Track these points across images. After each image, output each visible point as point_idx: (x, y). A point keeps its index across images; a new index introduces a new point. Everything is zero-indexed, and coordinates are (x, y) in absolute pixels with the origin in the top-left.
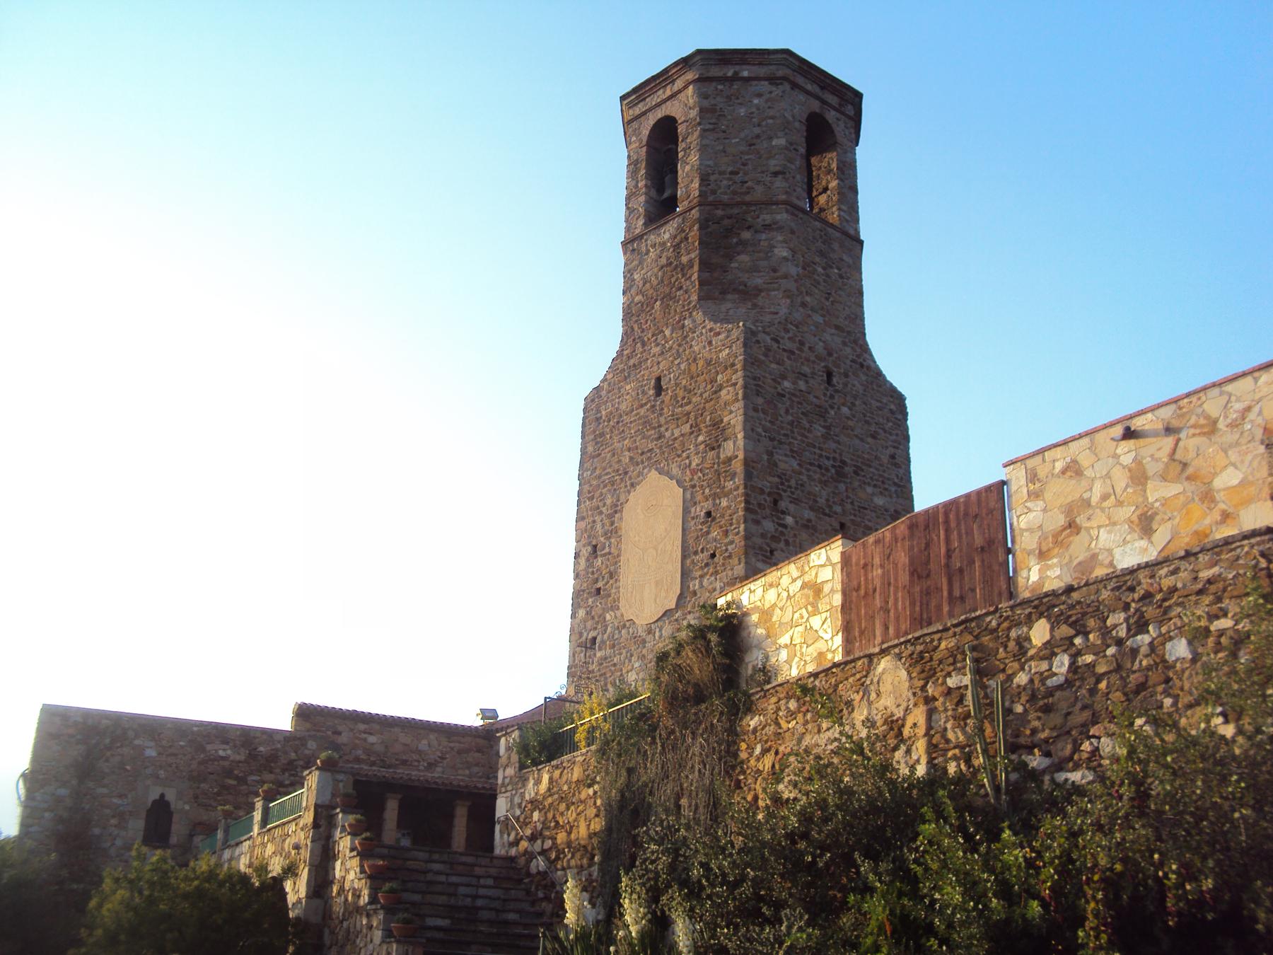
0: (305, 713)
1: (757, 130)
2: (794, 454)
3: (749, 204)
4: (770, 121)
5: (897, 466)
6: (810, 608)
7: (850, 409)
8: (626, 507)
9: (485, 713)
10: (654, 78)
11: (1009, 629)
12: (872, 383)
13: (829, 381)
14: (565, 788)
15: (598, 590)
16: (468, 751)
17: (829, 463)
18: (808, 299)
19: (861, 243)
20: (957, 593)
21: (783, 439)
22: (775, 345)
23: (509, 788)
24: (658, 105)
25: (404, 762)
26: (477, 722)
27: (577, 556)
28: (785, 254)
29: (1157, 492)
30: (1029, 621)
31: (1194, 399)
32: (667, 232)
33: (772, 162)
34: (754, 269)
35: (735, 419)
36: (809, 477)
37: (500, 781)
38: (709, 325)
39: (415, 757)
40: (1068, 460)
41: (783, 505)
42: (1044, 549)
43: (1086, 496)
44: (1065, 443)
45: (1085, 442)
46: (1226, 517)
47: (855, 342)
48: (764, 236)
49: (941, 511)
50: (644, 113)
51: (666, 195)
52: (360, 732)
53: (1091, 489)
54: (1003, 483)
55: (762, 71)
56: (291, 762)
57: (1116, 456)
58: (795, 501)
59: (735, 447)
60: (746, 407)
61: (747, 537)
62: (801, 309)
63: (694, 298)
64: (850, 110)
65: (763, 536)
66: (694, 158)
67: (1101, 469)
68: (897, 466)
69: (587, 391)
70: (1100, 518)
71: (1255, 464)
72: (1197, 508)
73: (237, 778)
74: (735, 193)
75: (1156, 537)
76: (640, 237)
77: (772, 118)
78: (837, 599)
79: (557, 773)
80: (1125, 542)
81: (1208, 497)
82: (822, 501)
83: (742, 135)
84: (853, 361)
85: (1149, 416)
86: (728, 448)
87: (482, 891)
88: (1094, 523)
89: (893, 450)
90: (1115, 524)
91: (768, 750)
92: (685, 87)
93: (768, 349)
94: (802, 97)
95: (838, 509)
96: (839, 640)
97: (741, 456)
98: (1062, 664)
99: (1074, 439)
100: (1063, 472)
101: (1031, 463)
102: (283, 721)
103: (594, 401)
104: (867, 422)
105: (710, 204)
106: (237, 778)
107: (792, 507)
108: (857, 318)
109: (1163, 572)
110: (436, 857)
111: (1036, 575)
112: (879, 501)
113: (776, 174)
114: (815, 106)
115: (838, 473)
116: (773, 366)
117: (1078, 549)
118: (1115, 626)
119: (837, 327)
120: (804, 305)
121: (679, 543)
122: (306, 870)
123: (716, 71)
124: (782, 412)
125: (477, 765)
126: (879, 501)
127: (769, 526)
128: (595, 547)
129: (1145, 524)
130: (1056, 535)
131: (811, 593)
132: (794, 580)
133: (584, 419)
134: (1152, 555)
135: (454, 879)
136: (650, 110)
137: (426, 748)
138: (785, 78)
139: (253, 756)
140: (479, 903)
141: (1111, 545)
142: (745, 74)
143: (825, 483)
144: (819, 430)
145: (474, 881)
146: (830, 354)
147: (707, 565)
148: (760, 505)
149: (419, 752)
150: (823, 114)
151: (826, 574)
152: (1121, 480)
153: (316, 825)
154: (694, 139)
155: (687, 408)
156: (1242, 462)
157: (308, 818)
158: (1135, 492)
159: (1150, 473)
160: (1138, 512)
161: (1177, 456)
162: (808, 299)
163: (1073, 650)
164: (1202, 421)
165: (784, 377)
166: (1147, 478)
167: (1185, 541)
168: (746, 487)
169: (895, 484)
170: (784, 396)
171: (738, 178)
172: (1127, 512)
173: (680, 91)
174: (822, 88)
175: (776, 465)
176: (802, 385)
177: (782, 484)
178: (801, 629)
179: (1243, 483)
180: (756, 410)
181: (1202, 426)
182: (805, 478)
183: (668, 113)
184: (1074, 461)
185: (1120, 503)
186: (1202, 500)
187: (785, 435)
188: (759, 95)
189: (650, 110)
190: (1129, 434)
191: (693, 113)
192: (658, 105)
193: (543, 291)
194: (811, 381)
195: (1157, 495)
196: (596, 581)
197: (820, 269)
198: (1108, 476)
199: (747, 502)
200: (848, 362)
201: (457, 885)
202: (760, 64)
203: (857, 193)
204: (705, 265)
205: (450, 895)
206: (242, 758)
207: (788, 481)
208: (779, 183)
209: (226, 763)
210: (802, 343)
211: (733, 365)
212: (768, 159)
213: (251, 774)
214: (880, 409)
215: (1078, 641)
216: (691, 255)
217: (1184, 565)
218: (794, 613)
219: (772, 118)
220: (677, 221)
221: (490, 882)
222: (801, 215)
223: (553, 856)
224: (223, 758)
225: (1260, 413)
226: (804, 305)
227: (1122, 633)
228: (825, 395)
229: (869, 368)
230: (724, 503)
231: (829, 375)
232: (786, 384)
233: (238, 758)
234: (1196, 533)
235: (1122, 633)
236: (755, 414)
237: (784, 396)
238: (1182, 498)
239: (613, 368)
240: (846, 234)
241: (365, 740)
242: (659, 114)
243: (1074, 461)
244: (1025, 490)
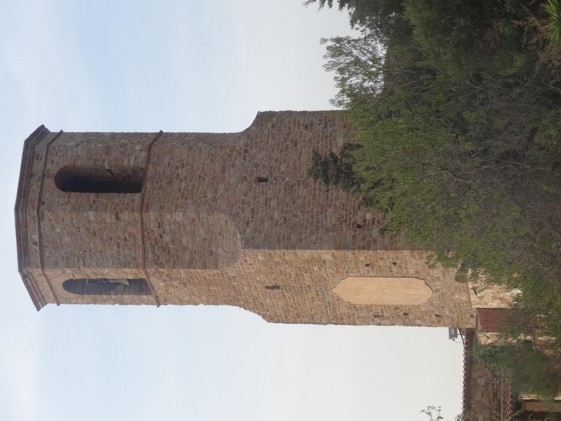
1: (83, 230)
3: (143, 232)
4: (74, 221)
7: (281, 163)
8: (352, 302)
10: (30, 294)
12: (256, 143)
13: (265, 180)
15: (404, 314)
21: (315, 219)
22: (251, 224)
25: (495, 395)
27: (380, 325)
28: (181, 214)
32: (154, 281)
33: (108, 220)
35: (306, 254)
36: (337, 199)
38: (237, 265)
39: (490, 387)
41: (360, 222)
48: (167, 228)
59: (326, 255)
60: (300, 248)
62: (219, 202)
63: (215, 271)
69: (265, 322)
74: (134, 245)
76: (157, 297)
77: (72, 219)
84: (244, 159)
89: (301, 127)
93: (255, 230)
103: (272, 317)
104: (287, 148)
105: (144, 261)
113: (118, 218)
114: (50, 183)
116: (266, 225)
119: (223, 172)
120: (215, 199)
121: (383, 279)
124: (297, 220)
128: (375, 316)
137: (483, 379)
142: (36, 237)
147: (400, 267)
148: (364, 239)
165: (272, 218)
168: (354, 249)
169: (325, 127)
170: (285, 219)
171: (122, 243)
174: (31, 176)
175: (334, 226)
176: (273, 203)
177: (346, 221)
180: (301, 240)
182: (338, 203)
187: (312, 218)
188: (53, 228)
194: (269, 195)
196: (399, 316)
197: (183, 184)
199: (363, 248)
200: (246, 163)
204: (190, 265)
207: (343, 217)
212: (105, 223)
219: (72, 219)
220: (152, 279)
222: (146, 200)
226: (215, 199)
228: (276, 184)
231: (261, 180)
232: (276, 216)
236: (304, 241)
237: (285, 219)
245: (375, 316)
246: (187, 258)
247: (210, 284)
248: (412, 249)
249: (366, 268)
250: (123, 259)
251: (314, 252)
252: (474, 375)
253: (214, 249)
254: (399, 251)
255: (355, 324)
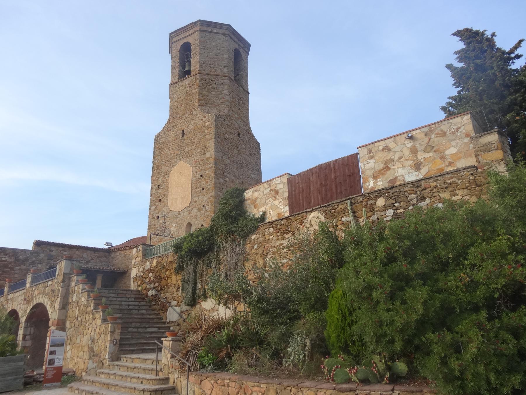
0: (38, 244)
1: (219, 51)
2: (229, 158)
3: (215, 75)
5: (257, 165)
6: (273, 198)
9: (108, 244)
10: (183, 28)
11: (367, 201)
14: (165, 264)
15: (160, 200)
16: (101, 257)
17: (239, 162)
18: (234, 109)
19: (249, 93)
20: (339, 191)
23: (138, 265)
24: (184, 38)
26: (105, 247)
27: (152, 189)
29: (421, 156)
30: (376, 198)
31: (437, 125)
32: (187, 81)
34: (217, 97)
35: (211, 144)
36: (233, 166)
37: (133, 263)
40: (385, 146)
41: (225, 174)
42: (375, 175)
43: (392, 158)
44: (383, 140)
45: (392, 139)
46: (450, 164)
47: (246, 125)
49: (332, 164)
50: (178, 40)
51: (186, 69)
52: (61, 251)
53: (394, 155)
54: (357, 154)
55: (221, 31)
56: (33, 262)
57: (404, 144)
58: (229, 173)
59: (211, 154)
61: (215, 184)
64: (246, 49)
65: (220, 184)
66: (197, 57)
67: (398, 149)
68: (257, 165)
70: (398, 165)
71: (462, 146)
72: (438, 161)
73: (9, 268)
75: (422, 171)
76: (177, 83)
78: (286, 195)
79: (160, 259)
80: (409, 173)
81: (443, 158)
82: (237, 174)
83: (214, 52)
85: (418, 131)
86: (208, 155)
87: (131, 303)
88: (396, 167)
90: (405, 167)
91: (260, 247)
92: (194, 33)
94: (233, 42)
95: (241, 177)
96: (287, 208)
97: (213, 157)
98: (390, 212)
99: (387, 139)
100: (383, 150)
101: (369, 147)
102: (29, 246)
103: (158, 138)
106: (9, 268)
107: (228, 175)
108: (247, 117)
109: (431, 181)
110: (111, 291)
111: (370, 184)
112: (253, 176)
113: (225, 66)
114: (237, 46)
115: (241, 166)
117: (390, 176)
118: (412, 199)
119: (242, 119)
122: (59, 299)
123: (205, 28)
125: (104, 262)
126: (253, 176)
127: (221, 180)
128: (159, 186)
129: (417, 167)
130: (380, 171)
131: (273, 193)
132: (266, 189)
133: (155, 143)
134: (421, 177)
135: (119, 299)
136: (181, 39)
138: (228, 34)
139: (17, 259)
140: (131, 307)
141: (404, 174)
142: (215, 31)
143: (237, 168)
144: (236, 151)
145: (127, 299)
146: (240, 128)
147: (200, 192)
149: (83, 258)
150: (238, 50)
151: (281, 186)
152: (407, 153)
153: (63, 281)
154: (197, 50)
155: (194, 141)
156: (457, 145)
157: (60, 278)
158: (413, 156)
159: (419, 150)
160: (415, 163)
161: (430, 144)
162: (234, 109)
163: (394, 208)
164: (440, 132)
166: (417, 151)
167: (434, 173)
171: (212, 66)
172: (411, 162)
173: (192, 34)
178: (269, 205)
179: (457, 153)
181: (440, 134)
183: (190, 41)
184: (387, 146)
185: (407, 160)
186: (441, 158)
188: (220, 39)
189: (181, 39)
190: (411, 138)
191: (197, 42)
192: (184, 38)
193: (147, 97)
195: (422, 157)
196: (159, 197)
198: (401, 151)
199: (215, 172)
201: (121, 301)
202: (220, 28)
203: (248, 77)
204: (200, 94)
205: (120, 305)
206: (12, 260)
208: (225, 69)
209: (5, 263)
210: (231, 123)
211: (210, 127)
213: (17, 266)
214: (253, 147)
215: (397, 205)
216: (196, 90)
217: (439, 178)
218: (266, 200)
220: (191, 78)
221: (133, 299)
223: (159, 289)
224: (4, 261)
225: (464, 129)
226: (232, 111)
227: (415, 201)
229: (250, 134)
230: (207, 172)
231: (239, 134)
232: (227, 135)
233: (10, 260)
234: (438, 169)
235: (415, 201)
238: (432, 158)
239: (166, 126)
240: (245, 90)
241: (62, 253)
242: (185, 41)
243: (387, 146)
244: (367, 156)
245: (159, 186)
246: (204, 93)
247: (186, 104)
248: (215, 197)
249: (199, 175)
250: (203, 65)
251: (213, 147)
252: (88, 252)
253: (209, 105)
254: (214, 191)
255: (152, 176)
